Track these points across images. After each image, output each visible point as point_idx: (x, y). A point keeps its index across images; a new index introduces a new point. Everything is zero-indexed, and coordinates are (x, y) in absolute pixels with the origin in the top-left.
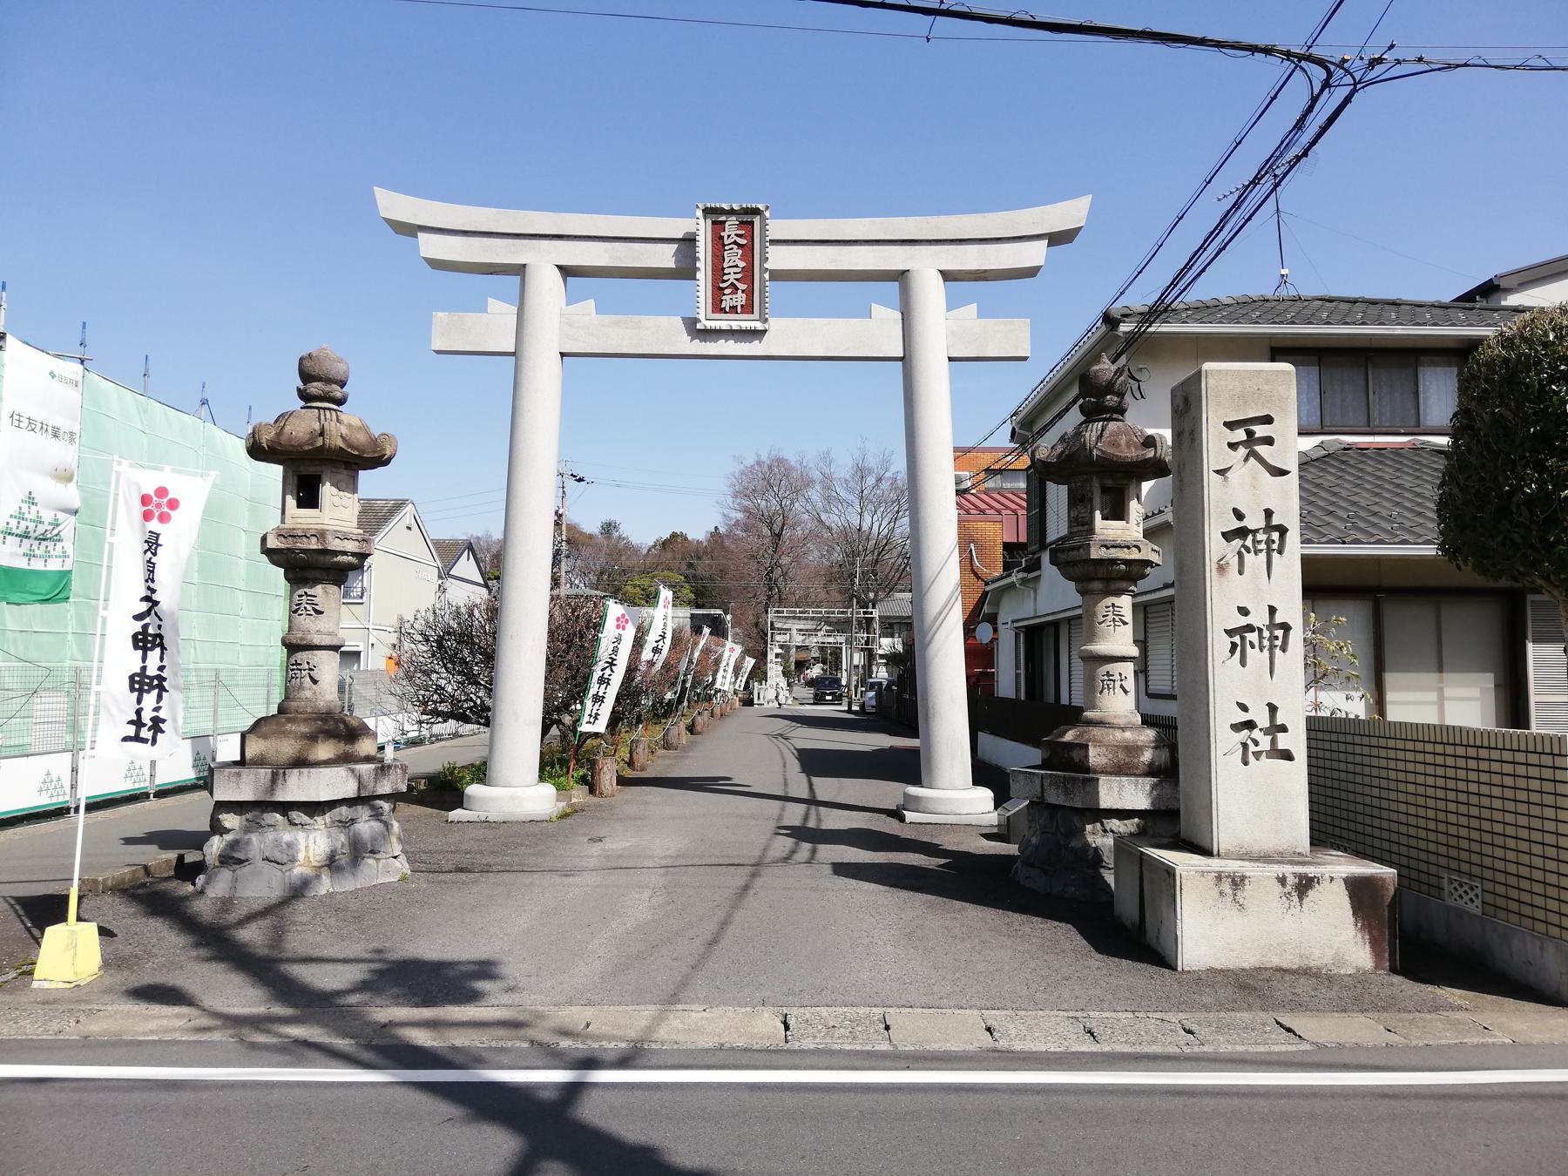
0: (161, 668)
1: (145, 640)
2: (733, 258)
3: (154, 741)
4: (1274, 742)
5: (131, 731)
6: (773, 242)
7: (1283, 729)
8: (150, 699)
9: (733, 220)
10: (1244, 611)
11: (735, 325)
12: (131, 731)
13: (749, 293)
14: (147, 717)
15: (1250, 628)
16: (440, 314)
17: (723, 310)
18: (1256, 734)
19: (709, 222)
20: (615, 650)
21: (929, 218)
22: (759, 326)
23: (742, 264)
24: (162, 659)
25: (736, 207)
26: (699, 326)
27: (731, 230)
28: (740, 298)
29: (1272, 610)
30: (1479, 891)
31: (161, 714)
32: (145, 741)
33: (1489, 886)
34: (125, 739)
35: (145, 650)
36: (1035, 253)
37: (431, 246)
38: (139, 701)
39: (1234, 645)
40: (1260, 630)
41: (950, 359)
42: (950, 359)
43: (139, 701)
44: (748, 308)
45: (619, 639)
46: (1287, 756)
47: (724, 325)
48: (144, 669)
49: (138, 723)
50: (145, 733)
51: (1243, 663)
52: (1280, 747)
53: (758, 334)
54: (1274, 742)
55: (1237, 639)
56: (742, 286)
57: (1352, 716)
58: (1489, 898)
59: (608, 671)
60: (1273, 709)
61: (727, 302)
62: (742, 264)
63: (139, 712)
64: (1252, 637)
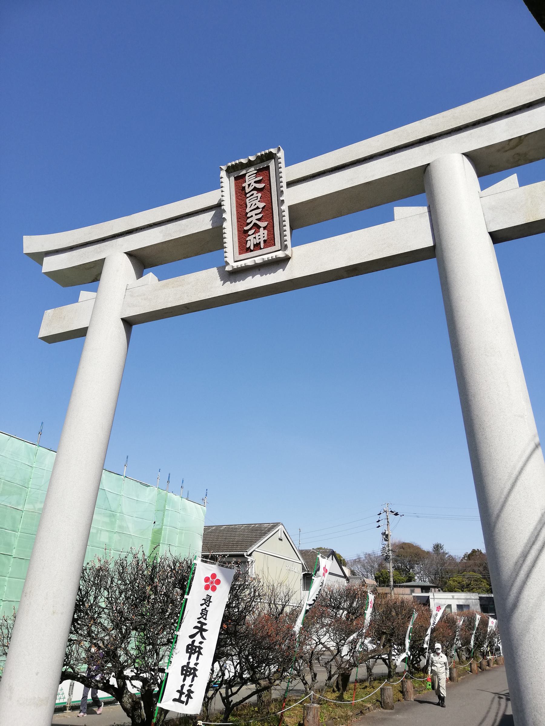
0: (196, 664)
2: (255, 202)
5: (177, 696)
6: (290, 184)
9: (252, 170)
11: (258, 260)
12: (177, 696)
13: (270, 228)
14: (185, 690)
16: (49, 311)
17: (248, 250)
19: (232, 179)
20: (204, 613)
22: (281, 254)
23: (261, 205)
25: (252, 158)
26: (228, 268)
27: (251, 178)
28: (263, 234)
31: (192, 689)
32: (182, 702)
34: (175, 700)
35: (191, 654)
37: (51, 264)
41: (497, 237)
42: (497, 237)
44: (269, 242)
45: (208, 601)
47: (249, 262)
48: (188, 663)
50: (184, 698)
53: (283, 262)
56: (263, 224)
59: (198, 638)
63: (183, 686)
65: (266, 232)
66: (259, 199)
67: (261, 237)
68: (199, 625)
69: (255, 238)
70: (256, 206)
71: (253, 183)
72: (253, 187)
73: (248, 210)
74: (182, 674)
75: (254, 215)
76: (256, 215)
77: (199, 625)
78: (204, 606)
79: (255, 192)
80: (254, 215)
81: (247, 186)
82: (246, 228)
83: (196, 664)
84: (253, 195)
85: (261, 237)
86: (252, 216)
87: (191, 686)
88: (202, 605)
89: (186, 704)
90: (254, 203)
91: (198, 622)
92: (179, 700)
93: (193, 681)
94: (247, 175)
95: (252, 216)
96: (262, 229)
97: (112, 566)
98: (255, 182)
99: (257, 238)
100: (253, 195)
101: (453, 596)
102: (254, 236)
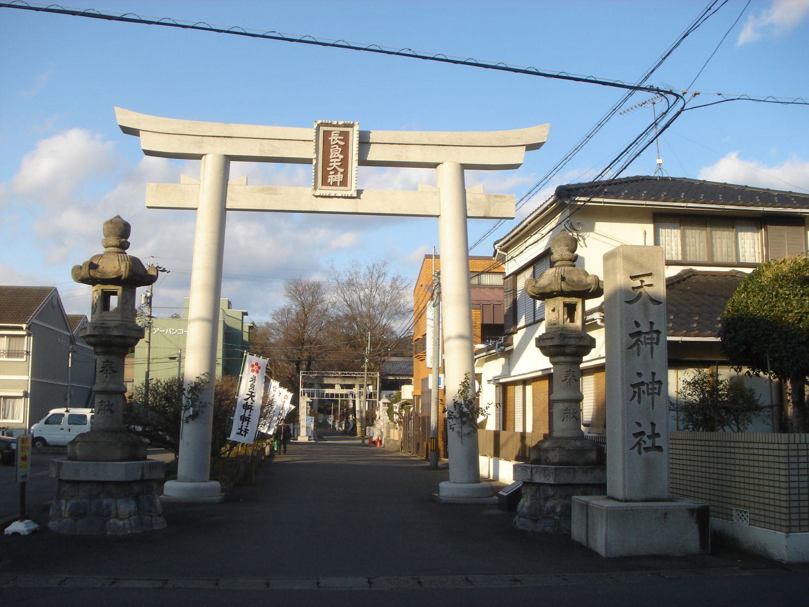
1: (246, 406)
3: (245, 436)
4: (653, 443)
7: (658, 435)
8: (245, 423)
10: (639, 374)
13: (345, 174)
14: (243, 429)
15: (642, 383)
17: (329, 184)
18: (645, 438)
21: (455, 133)
23: (341, 157)
24: (250, 412)
28: (339, 177)
29: (653, 374)
30: (748, 514)
31: (248, 428)
32: (242, 435)
33: (752, 510)
34: (237, 433)
36: (517, 156)
38: (242, 424)
39: (635, 392)
40: (647, 384)
43: (242, 424)
46: (659, 449)
48: (245, 414)
49: (241, 429)
50: (243, 433)
51: (639, 402)
52: (657, 445)
54: (653, 443)
55: (636, 390)
57: (358, 152)
58: (752, 516)
60: (653, 424)
61: (331, 179)
62: (341, 157)
64: (644, 388)
65: (342, 176)
66: (339, 152)
67: (339, 178)
68: (250, 393)
69: (334, 177)
70: (337, 156)
71: (336, 140)
72: (336, 142)
73: (331, 157)
74: (241, 420)
75: (335, 162)
76: (336, 162)
77: (250, 393)
78: (252, 382)
79: (337, 146)
80: (335, 162)
81: (332, 141)
82: (328, 169)
83: (250, 415)
84: (335, 147)
85: (339, 178)
86: (333, 162)
87: (247, 427)
88: (250, 381)
89: (245, 436)
90: (336, 153)
91: (249, 391)
92: (240, 434)
93: (248, 424)
94: (333, 132)
95: (333, 162)
96: (339, 173)
97: (458, 399)
98: (338, 139)
99: (336, 178)
100: (335, 147)
101: (742, 248)
102: (333, 176)
